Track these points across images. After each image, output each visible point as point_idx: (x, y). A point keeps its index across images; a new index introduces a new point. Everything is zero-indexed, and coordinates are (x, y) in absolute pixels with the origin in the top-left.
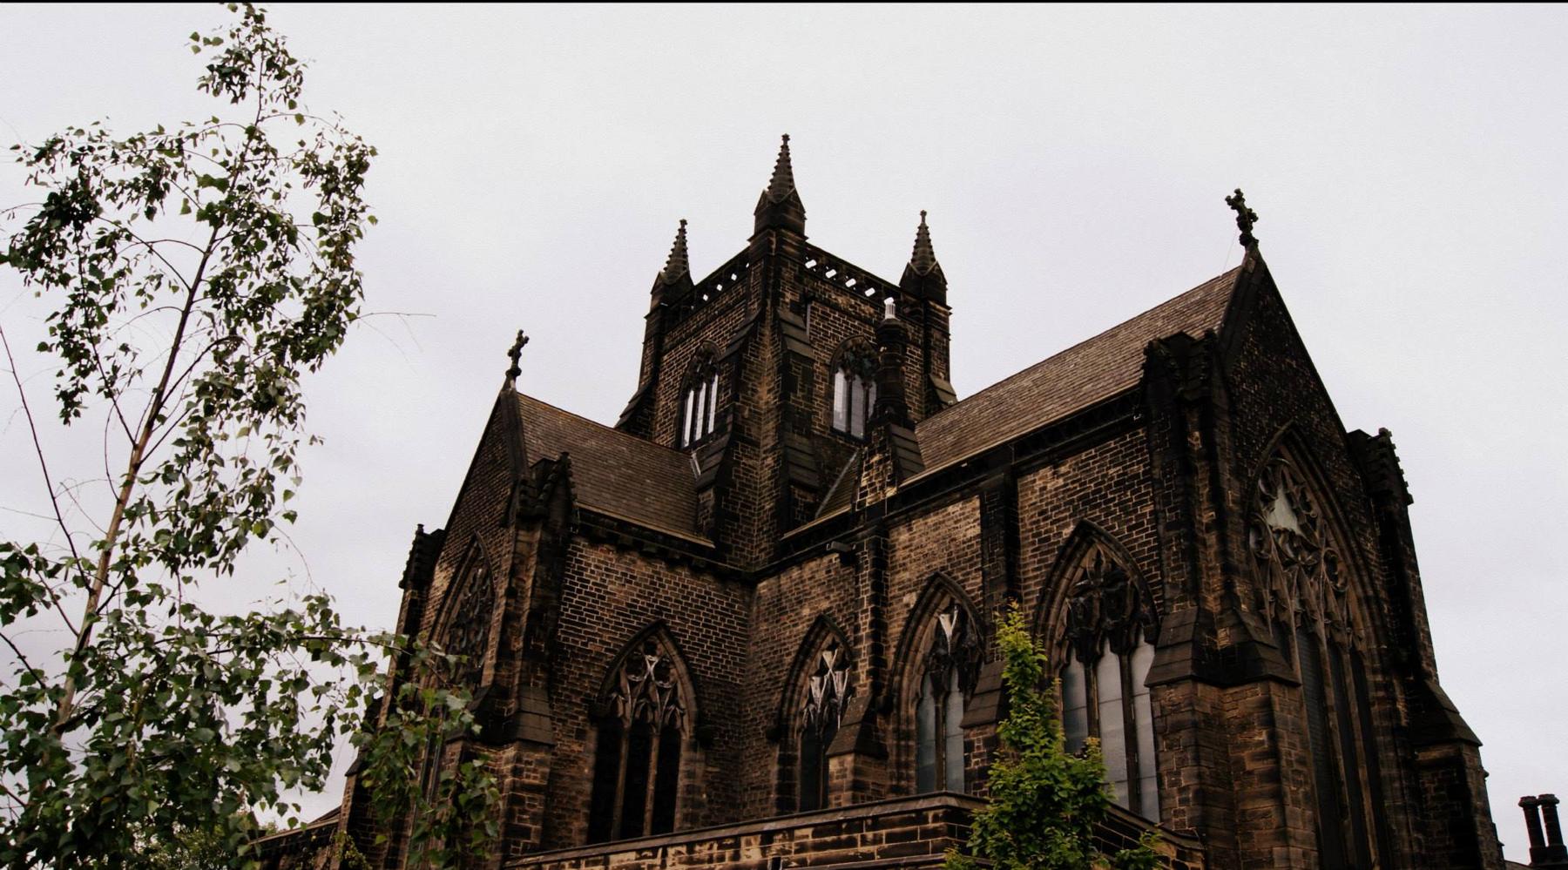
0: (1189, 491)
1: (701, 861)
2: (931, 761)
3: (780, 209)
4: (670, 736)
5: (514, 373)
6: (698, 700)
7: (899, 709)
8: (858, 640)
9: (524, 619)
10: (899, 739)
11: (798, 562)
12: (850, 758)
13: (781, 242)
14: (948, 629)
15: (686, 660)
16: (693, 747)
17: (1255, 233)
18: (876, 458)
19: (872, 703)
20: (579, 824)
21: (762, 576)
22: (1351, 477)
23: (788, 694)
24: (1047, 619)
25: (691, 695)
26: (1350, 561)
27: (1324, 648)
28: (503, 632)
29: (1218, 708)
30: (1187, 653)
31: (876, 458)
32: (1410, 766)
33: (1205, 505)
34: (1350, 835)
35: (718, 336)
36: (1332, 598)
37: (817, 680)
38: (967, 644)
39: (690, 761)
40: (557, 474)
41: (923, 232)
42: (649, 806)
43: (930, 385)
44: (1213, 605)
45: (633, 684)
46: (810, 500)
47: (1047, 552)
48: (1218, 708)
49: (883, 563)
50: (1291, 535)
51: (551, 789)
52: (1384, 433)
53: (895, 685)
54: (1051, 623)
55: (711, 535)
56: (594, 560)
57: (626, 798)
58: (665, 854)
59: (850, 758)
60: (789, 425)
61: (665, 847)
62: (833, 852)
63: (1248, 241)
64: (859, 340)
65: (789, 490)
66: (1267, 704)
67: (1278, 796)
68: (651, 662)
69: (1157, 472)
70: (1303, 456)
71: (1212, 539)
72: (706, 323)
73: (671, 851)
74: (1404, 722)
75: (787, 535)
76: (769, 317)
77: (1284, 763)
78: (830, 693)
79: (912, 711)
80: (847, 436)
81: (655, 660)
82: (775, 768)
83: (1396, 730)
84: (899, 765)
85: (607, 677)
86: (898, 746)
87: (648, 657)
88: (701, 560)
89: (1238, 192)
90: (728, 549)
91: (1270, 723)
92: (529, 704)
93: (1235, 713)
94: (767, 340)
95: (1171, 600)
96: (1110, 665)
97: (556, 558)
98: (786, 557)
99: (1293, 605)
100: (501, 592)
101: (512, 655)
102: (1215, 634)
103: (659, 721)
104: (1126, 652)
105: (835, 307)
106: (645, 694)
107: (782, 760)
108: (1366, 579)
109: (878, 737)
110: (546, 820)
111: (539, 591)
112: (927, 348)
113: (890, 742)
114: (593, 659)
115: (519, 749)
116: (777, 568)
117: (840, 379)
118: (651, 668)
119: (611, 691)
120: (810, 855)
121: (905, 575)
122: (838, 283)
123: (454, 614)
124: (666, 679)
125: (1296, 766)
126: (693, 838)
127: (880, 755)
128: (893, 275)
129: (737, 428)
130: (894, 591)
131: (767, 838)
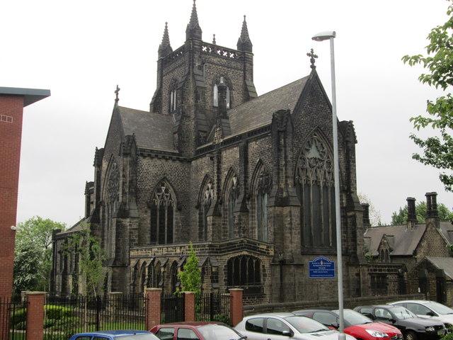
3: (194, 31)
4: (170, 208)
5: (117, 100)
13: (194, 44)
14: (235, 182)
15: (173, 187)
19: (217, 202)
20: (148, 236)
25: (175, 197)
28: (123, 187)
30: (274, 199)
35: (179, 74)
40: (132, 140)
41: (245, 23)
42: (166, 228)
43: (245, 83)
44: (283, 186)
49: (219, 162)
50: (315, 159)
51: (139, 229)
55: (178, 148)
56: (144, 162)
57: (164, 214)
63: (313, 67)
66: (290, 212)
67: (291, 233)
68: (163, 189)
71: (284, 169)
76: (191, 73)
78: (210, 196)
82: (198, 216)
88: (174, 157)
89: (312, 50)
92: (132, 207)
97: (135, 164)
98: (200, 154)
100: (121, 175)
105: (213, 63)
106: (162, 198)
107: (199, 214)
110: (139, 236)
112: (244, 70)
116: (196, 158)
122: (214, 54)
124: (168, 193)
127: (220, 215)
130: (223, 170)
131: (181, 247)
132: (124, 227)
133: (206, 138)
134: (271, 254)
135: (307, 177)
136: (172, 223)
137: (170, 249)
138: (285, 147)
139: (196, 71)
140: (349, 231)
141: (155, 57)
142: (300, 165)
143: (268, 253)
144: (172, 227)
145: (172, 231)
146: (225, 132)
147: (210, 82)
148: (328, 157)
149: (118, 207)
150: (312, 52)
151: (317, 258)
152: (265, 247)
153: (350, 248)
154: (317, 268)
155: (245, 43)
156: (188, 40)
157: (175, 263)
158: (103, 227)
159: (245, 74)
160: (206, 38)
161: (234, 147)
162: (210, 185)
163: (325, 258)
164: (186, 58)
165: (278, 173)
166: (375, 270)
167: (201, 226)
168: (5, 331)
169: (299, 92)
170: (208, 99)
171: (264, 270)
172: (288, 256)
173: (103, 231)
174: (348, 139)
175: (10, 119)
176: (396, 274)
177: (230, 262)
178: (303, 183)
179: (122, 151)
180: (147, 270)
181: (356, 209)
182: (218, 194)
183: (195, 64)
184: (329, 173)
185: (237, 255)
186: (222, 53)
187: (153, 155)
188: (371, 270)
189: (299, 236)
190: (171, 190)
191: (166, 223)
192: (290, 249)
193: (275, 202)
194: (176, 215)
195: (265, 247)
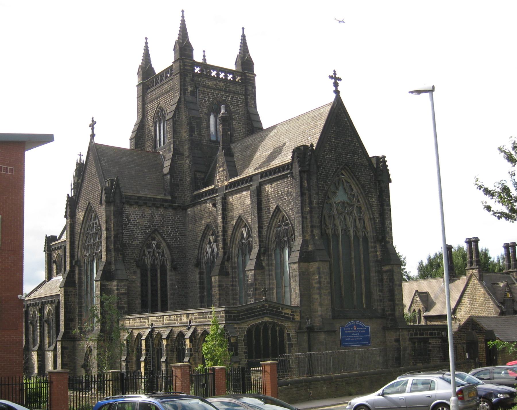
1: (172, 320)
2: (242, 276)
3: (184, 48)
4: (163, 267)
5: (93, 136)
6: (171, 254)
7: (232, 259)
9: (112, 238)
10: (232, 269)
12: (217, 277)
14: (245, 233)
16: (171, 271)
18: (221, 169)
19: (224, 258)
20: (138, 301)
21: (189, 206)
24: (270, 235)
25: (169, 253)
31: (221, 169)
37: (208, 245)
39: (170, 276)
41: (244, 37)
43: (248, 112)
44: (308, 237)
45: (149, 252)
46: (203, 176)
50: (344, 203)
51: (127, 294)
54: (271, 236)
55: (171, 194)
56: (131, 211)
58: (163, 318)
61: (163, 316)
62: (203, 320)
63: (337, 92)
64: (218, 99)
65: (195, 174)
67: (320, 294)
70: (350, 174)
71: (308, 217)
73: (165, 317)
75: (196, 193)
76: (183, 100)
77: (322, 285)
78: (213, 251)
79: (236, 260)
81: (155, 242)
82: (198, 276)
83: (377, 261)
84: (233, 277)
85: (141, 252)
86: (232, 271)
87: (153, 242)
89: (335, 71)
90: (176, 198)
94: (183, 110)
101: (110, 251)
102: (308, 246)
105: (208, 87)
106: (154, 255)
108: (370, 212)
112: (246, 95)
113: (230, 270)
114: (136, 247)
115: (118, 282)
116: (194, 205)
118: (154, 246)
119: (143, 256)
133: (203, 179)
134: (296, 320)
135: (335, 225)
136: (166, 285)
137: (173, 318)
138: (309, 189)
141: (133, 80)
142: (325, 212)
143: (294, 319)
144: (166, 291)
145: (166, 295)
147: (205, 110)
148: (358, 201)
149: (101, 268)
150: (335, 74)
151: (350, 323)
152: (289, 312)
153: (386, 309)
154: (350, 334)
155: (245, 62)
157: (181, 335)
159: (246, 99)
160: (198, 57)
161: (242, 191)
162: (212, 238)
163: (359, 322)
166: (416, 334)
167: (202, 288)
169: (321, 123)
170: (204, 131)
171: (289, 339)
172: (317, 322)
174: (380, 178)
175: (11, 171)
176: (439, 338)
177: (249, 331)
178: (330, 231)
180: (144, 343)
181: (392, 263)
182: (224, 248)
183: (187, 90)
186: (218, 74)
187: (141, 202)
188: (411, 335)
189: (330, 297)
190: (163, 244)
191: (159, 286)
193: (300, 257)
194: (170, 276)
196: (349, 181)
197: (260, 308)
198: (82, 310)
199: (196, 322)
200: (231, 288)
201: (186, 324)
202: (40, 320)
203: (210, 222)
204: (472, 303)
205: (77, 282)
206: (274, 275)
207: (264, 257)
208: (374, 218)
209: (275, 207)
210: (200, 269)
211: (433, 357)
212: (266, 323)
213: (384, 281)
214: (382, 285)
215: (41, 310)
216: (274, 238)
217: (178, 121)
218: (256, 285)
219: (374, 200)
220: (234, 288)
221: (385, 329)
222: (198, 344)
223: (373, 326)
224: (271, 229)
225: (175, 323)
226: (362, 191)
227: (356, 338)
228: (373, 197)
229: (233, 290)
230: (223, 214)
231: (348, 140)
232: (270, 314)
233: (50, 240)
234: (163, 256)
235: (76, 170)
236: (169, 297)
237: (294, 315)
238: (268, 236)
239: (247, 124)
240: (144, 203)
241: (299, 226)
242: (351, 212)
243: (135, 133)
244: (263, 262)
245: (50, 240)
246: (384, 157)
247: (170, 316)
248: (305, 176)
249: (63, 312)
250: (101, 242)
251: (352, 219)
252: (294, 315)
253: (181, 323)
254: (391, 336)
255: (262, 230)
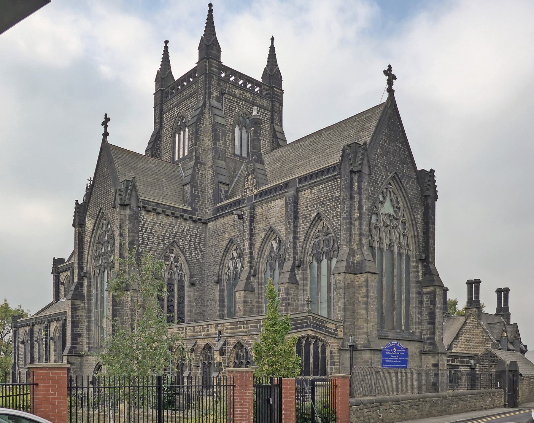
0: (351, 206)
3: (209, 46)
4: (181, 281)
5: (106, 135)
7: (258, 275)
8: (244, 250)
11: (222, 216)
17: (394, 87)
18: (250, 177)
19: (250, 273)
21: (210, 220)
22: (416, 189)
23: (221, 267)
24: (306, 246)
26: (410, 223)
27: (396, 255)
28: (120, 250)
29: (353, 281)
30: (344, 264)
31: (250, 177)
32: (420, 293)
33: (356, 212)
34: (395, 317)
36: (402, 237)
37: (231, 261)
38: (280, 253)
41: (272, 49)
43: (274, 129)
44: (355, 246)
46: (226, 189)
47: (307, 222)
48: (353, 281)
50: (390, 215)
52: (432, 171)
53: (257, 266)
54: (307, 247)
55: (191, 205)
56: (148, 218)
58: (186, 329)
59: (242, 292)
60: (217, 157)
61: (186, 327)
63: (391, 91)
64: (244, 111)
65: (218, 185)
66: (367, 281)
67: (367, 309)
69: (342, 198)
70: (398, 184)
71: (357, 223)
72: (181, 102)
74: (420, 279)
75: (218, 205)
76: (207, 104)
77: (369, 299)
78: (236, 267)
79: (263, 275)
80: (241, 156)
82: (218, 293)
83: (418, 282)
87: (171, 255)
88: (186, 216)
89: (390, 66)
90: (197, 210)
91: (367, 286)
93: (357, 283)
94: (207, 116)
95: (342, 245)
96: (325, 262)
97: (135, 219)
98: (219, 213)
99: (386, 241)
102: (355, 256)
103: (176, 278)
104: (330, 259)
105: (234, 96)
106: (171, 268)
108: (415, 229)
109: (252, 285)
111: (131, 234)
113: (256, 286)
117: (237, 129)
118: (172, 259)
120: (229, 331)
121: (260, 226)
123: (97, 238)
124: (177, 262)
125: (373, 299)
126: (195, 325)
128: (257, 73)
129: (197, 158)
130: (256, 231)
132: (123, 303)
133: (227, 192)
134: (339, 336)
136: (183, 302)
138: (360, 193)
139: (214, 103)
140: (425, 312)
143: (337, 335)
144: (183, 307)
146: (261, 181)
152: (333, 327)
153: (425, 332)
154: (389, 356)
155: (273, 73)
156: (201, 59)
157: (208, 348)
158: (89, 304)
164: (200, 84)
165: (350, 229)
168: (232, 418)
171: (332, 357)
172: (361, 341)
173: (89, 311)
176: (468, 366)
178: (376, 245)
179: (118, 201)
183: (213, 94)
184: (404, 236)
185: (303, 334)
190: (182, 258)
192: (365, 330)
194: (188, 291)
195: (333, 327)
196: (396, 192)
197: (304, 319)
198: (91, 324)
199: (227, 333)
200: (256, 305)
201: (215, 336)
202: (46, 338)
203: (235, 236)
204: (469, 341)
205: (85, 295)
206: (308, 290)
207: (298, 270)
208: (418, 236)
209: (314, 215)
210: (221, 286)
211: (461, 385)
212: (308, 337)
213: (424, 303)
214: (422, 307)
215: (47, 328)
216: (310, 250)
217: (201, 127)
218: (288, 299)
219: (419, 217)
220: (260, 305)
221: (422, 353)
222: (229, 358)
223: (412, 349)
224: (308, 240)
225: (201, 335)
226: (409, 205)
227: (395, 360)
228: (418, 214)
229: (258, 307)
230: (251, 225)
231: (399, 147)
232: (313, 327)
233: (57, 262)
234: (181, 270)
235: (85, 195)
236: (186, 314)
237: (337, 331)
238: (304, 247)
239: (273, 142)
240: (163, 211)
241: (346, 234)
242: (396, 227)
243: (152, 144)
244: (297, 276)
245: (57, 262)
246: (432, 171)
247: (194, 327)
248: (356, 177)
249: (70, 326)
250: (114, 251)
251: (397, 234)
252: (337, 331)
253: (208, 335)
254: (430, 360)
255: (297, 241)
